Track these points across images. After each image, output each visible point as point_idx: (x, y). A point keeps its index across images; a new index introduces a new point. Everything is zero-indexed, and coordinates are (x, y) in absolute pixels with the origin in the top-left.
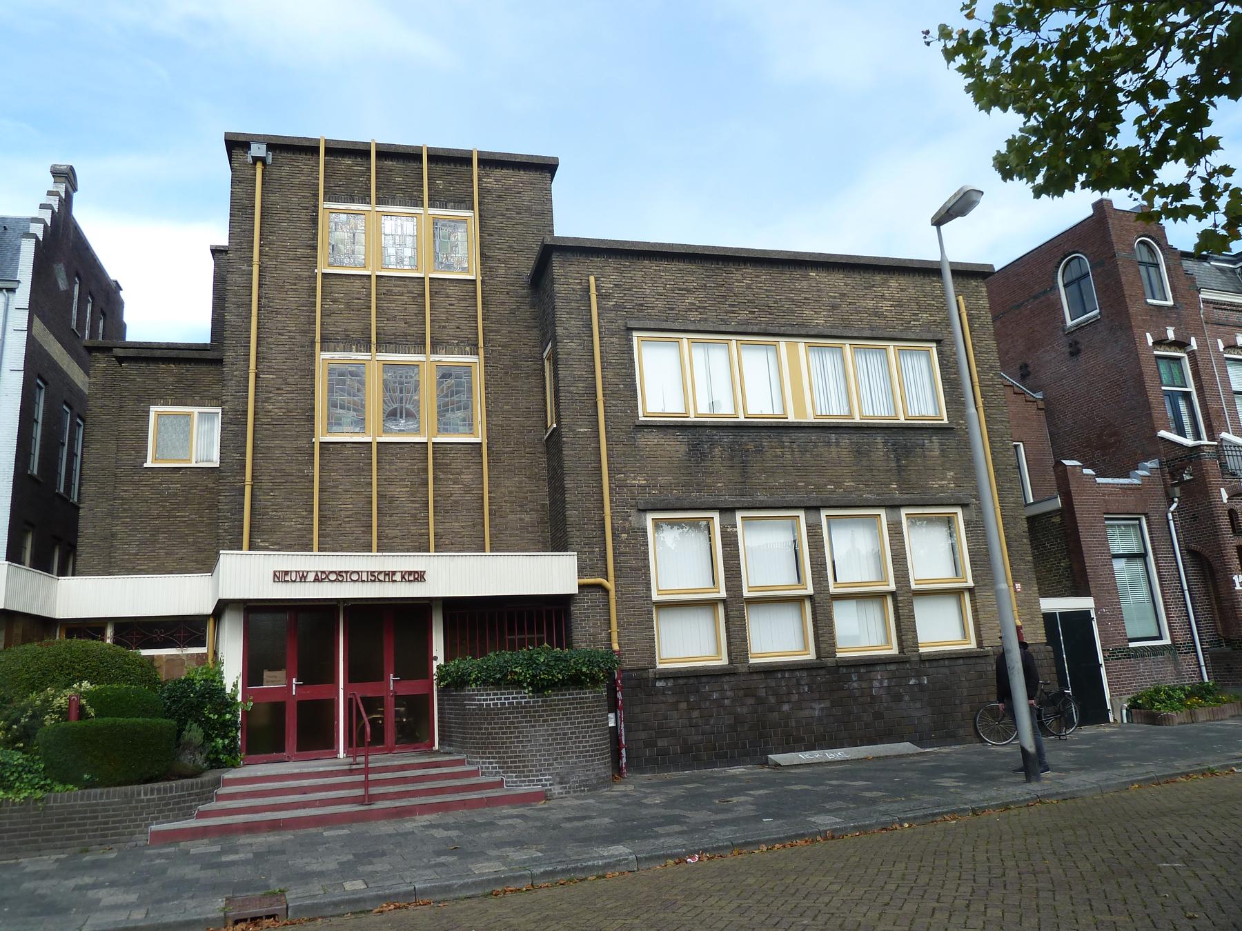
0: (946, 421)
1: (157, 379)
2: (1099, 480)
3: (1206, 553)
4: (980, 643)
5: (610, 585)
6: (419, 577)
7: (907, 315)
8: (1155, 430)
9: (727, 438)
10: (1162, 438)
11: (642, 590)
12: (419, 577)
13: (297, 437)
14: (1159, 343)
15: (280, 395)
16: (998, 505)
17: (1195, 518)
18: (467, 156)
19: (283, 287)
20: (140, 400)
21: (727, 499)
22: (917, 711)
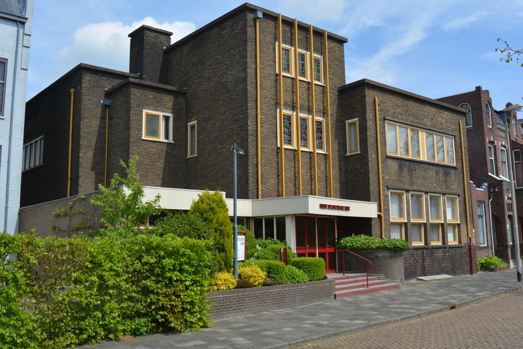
0: (455, 165)
1: (145, 96)
2: (477, 189)
3: (499, 216)
4: (460, 242)
5: (382, 215)
6: (347, 209)
7: (448, 125)
8: (487, 173)
9: (408, 164)
10: (490, 176)
11: (388, 217)
12: (347, 209)
13: (272, 145)
14: (502, 145)
15: (266, 125)
16: (251, 180)
17: (497, 204)
18: (322, 32)
19: (265, 77)
20: (139, 105)
21: (408, 187)
22: (447, 265)
